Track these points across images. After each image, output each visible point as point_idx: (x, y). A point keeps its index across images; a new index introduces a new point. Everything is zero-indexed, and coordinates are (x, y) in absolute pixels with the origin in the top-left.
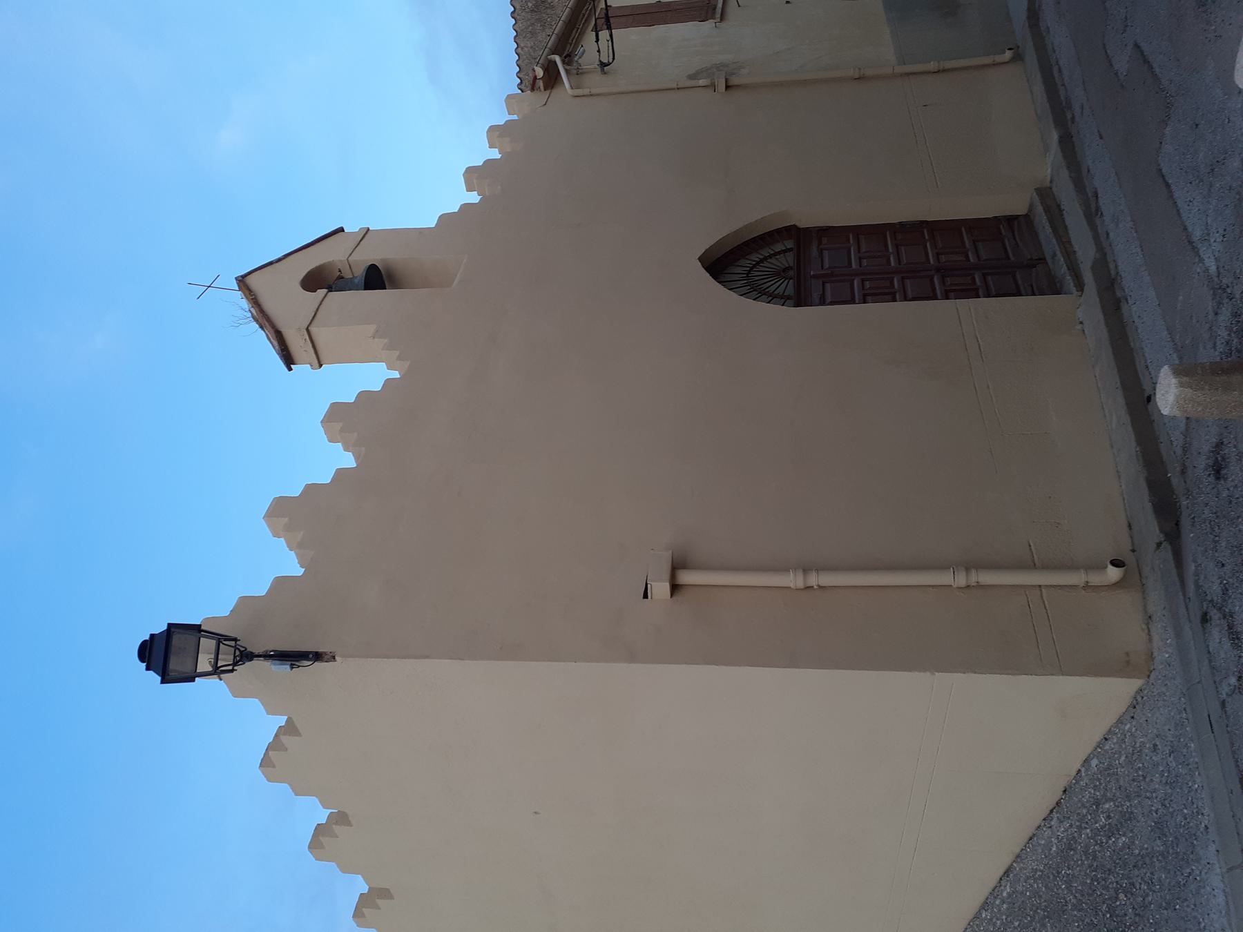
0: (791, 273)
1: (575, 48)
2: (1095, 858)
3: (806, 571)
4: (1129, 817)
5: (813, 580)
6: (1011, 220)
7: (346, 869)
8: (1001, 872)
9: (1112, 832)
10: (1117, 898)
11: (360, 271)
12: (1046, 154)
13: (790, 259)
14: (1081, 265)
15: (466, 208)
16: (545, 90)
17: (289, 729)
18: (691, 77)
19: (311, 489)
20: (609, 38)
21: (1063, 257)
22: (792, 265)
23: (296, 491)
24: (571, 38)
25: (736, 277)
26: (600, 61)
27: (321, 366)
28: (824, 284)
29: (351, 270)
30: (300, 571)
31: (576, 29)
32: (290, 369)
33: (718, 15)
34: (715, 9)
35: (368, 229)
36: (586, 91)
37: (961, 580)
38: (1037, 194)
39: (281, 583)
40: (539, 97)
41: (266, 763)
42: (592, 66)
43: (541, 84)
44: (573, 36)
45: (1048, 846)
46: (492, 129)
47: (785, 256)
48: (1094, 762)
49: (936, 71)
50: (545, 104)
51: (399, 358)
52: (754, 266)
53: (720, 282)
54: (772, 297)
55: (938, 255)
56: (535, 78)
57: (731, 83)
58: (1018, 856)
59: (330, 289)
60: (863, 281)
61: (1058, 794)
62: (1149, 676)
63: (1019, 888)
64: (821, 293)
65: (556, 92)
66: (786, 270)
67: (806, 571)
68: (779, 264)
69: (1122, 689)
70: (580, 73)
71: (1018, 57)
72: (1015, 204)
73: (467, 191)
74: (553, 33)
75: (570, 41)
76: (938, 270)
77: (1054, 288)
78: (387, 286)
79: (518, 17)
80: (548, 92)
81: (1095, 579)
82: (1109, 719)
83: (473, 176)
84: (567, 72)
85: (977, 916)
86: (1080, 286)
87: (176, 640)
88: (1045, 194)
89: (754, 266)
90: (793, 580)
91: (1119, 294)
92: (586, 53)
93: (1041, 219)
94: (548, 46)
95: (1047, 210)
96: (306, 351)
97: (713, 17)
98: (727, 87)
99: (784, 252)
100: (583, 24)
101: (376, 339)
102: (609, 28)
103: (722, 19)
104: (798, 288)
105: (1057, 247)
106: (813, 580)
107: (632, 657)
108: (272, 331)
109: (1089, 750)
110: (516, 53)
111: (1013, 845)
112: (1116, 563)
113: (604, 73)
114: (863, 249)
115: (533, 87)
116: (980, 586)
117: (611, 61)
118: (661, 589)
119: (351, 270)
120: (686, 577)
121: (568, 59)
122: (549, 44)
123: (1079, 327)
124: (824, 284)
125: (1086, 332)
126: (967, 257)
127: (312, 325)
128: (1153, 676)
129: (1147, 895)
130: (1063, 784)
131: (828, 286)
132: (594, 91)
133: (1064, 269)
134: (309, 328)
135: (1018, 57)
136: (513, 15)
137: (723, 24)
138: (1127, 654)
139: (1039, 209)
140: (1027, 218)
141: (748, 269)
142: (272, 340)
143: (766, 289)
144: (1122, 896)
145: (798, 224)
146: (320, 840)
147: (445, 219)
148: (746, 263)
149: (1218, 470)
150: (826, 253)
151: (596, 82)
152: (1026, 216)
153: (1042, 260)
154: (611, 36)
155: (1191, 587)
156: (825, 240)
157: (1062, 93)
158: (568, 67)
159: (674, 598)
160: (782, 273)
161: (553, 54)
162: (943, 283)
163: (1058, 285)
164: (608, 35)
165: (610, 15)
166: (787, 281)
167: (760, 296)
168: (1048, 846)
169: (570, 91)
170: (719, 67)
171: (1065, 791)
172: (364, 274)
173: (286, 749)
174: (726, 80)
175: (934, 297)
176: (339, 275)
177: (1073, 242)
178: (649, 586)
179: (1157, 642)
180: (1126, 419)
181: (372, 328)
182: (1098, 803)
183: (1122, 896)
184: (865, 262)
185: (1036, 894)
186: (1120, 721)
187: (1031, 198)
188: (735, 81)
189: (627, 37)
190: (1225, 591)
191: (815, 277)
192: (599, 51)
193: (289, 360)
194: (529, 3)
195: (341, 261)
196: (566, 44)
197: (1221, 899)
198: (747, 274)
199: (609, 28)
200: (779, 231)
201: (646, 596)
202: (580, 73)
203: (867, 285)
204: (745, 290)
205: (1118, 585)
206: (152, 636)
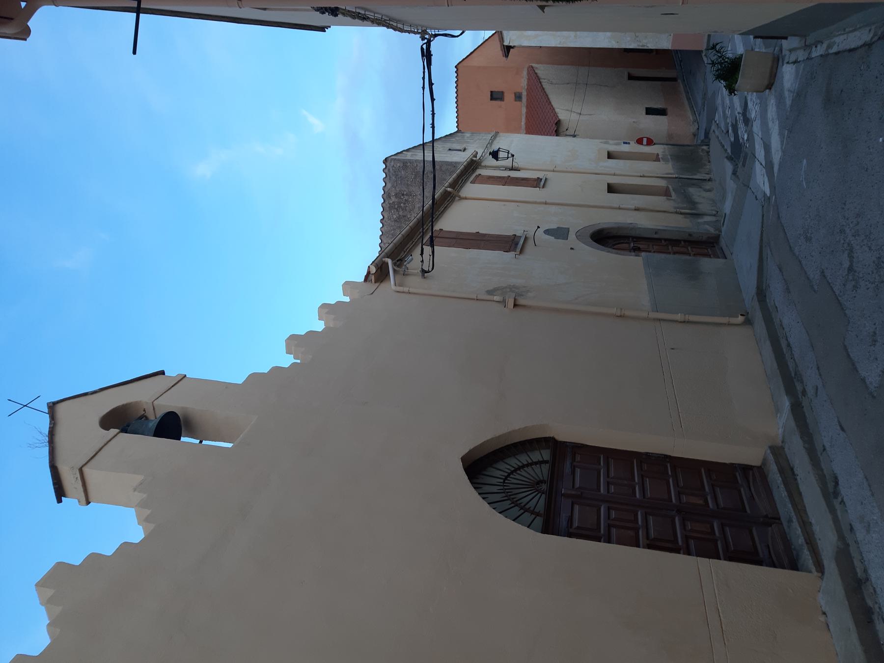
0: (544, 487)
12: (777, 414)
13: (544, 471)
14: (819, 542)
16: (375, 282)
18: (490, 292)
20: (431, 253)
21: (801, 528)
22: (546, 479)
24: (406, 248)
25: (494, 481)
26: (422, 269)
27: (88, 503)
29: (155, 412)
31: (411, 242)
32: (59, 501)
33: (518, 250)
34: (517, 244)
35: (185, 376)
36: (406, 289)
38: (772, 453)
40: (372, 286)
42: (416, 271)
43: (373, 278)
44: (408, 246)
46: (324, 306)
47: (540, 466)
49: (682, 321)
50: (372, 294)
52: (512, 472)
55: (679, 494)
57: (518, 303)
60: (609, 509)
65: (384, 286)
66: (540, 482)
68: (534, 475)
72: (755, 461)
73: (287, 353)
75: (405, 250)
79: (385, 223)
80: (377, 284)
84: (395, 271)
86: (820, 567)
88: (777, 451)
92: (413, 261)
93: (773, 470)
94: (385, 251)
95: (781, 471)
96: (76, 488)
97: (514, 250)
98: (515, 305)
100: (419, 239)
101: (136, 493)
102: (432, 246)
103: (521, 252)
105: (793, 514)
110: (380, 246)
113: (424, 277)
114: (612, 474)
117: (430, 270)
119: (155, 412)
122: (388, 249)
123: (822, 618)
125: (831, 627)
126: (706, 501)
131: (577, 507)
132: (411, 290)
133: (801, 540)
134: (83, 469)
135: (748, 322)
136: (382, 221)
137: (521, 257)
139: (771, 457)
141: (509, 471)
143: (519, 500)
145: (557, 438)
147: (254, 378)
150: (578, 471)
151: (415, 283)
152: (759, 468)
153: (777, 518)
154: (433, 252)
156: (578, 458)
157: (791, 365)
158: (396, 268)
161: (388, 258)
162: (683, 526)
163: (795, 553)
164: (431, 251)
166: (540, 494)
167: (513, 507)
169: (393, 287)
170: (512, 288)
174: (515, 300)
176: (143, 414)
177: (809, 514)
187: (765, 453)
188: (521, 301)
191: (567, 496)
192: (422, 261)
193: (60, 493)
194: (394, 216)
195: (147, 403)
198: (505, 480)
199: (432, 246)
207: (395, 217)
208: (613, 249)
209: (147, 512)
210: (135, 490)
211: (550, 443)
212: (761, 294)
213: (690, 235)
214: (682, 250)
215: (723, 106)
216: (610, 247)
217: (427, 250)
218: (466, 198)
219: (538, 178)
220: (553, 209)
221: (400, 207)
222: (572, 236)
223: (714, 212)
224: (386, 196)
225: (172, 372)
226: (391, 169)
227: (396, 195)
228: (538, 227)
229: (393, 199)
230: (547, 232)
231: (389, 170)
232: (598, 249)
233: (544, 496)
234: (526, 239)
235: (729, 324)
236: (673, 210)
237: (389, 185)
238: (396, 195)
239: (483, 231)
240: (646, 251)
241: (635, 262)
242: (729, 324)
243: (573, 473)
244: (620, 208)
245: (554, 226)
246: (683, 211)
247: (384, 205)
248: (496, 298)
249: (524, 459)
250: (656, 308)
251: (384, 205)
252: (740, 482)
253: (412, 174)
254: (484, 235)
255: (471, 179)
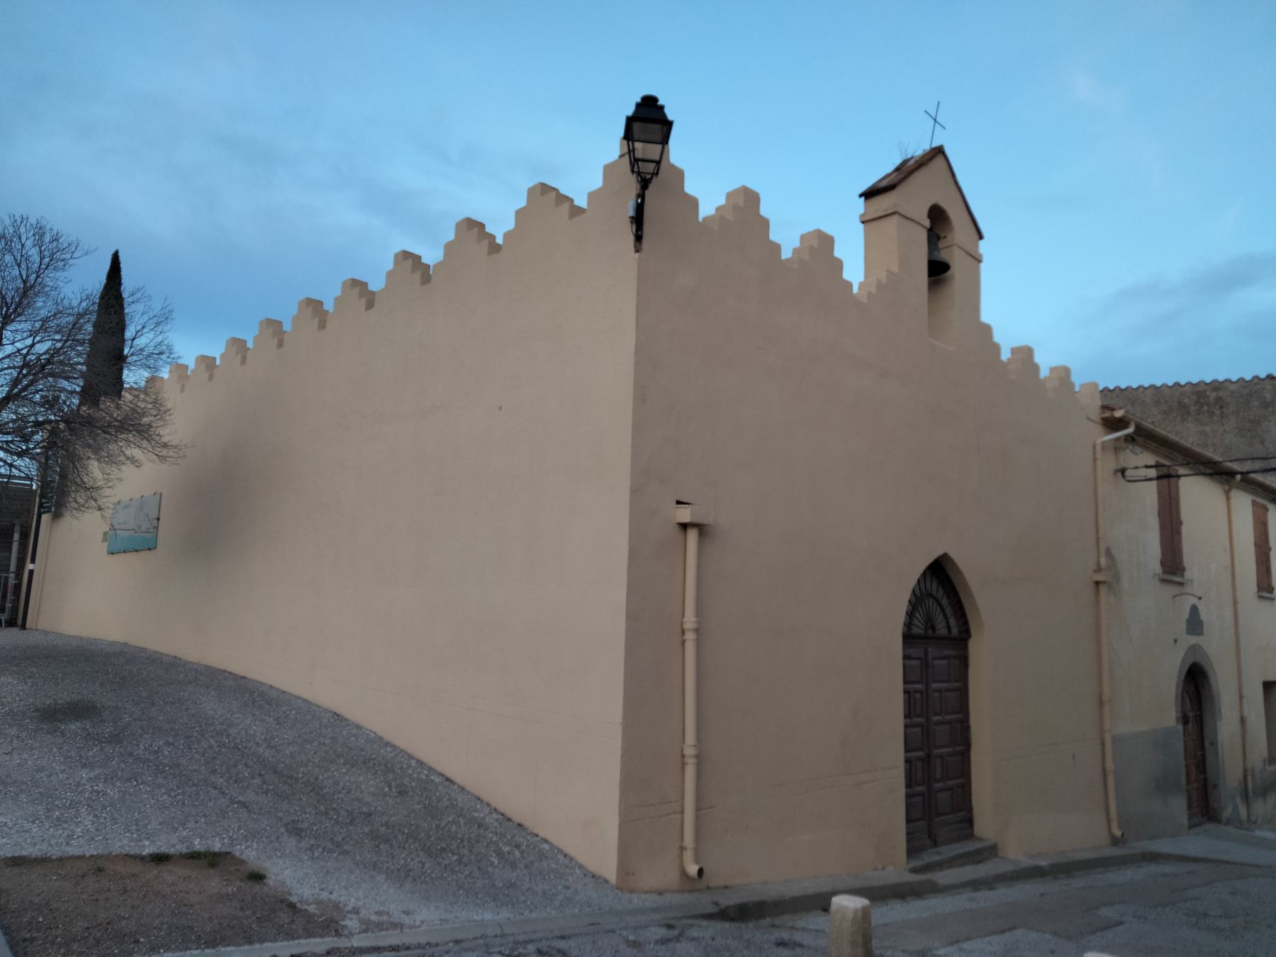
1: (1140, 446)
2: (478, 842)
3: (697, 630)
4: (513, 866)
5: (690, 636)
6: (970, 821)
7: (449, 247)
8: (448, 774)
9: (500, 854)
10: (453, 854)
11: (944, 255)
13: (942, 631)
15: (997, 348)
17: (576, 211)
18: (1108, 552)
19: (765, 223)
22: (938, 632)
23: (764, 211)
25: (928, 585)
27: (863, 222)
28: (920, 659)
30: (700, 219)
32: (861, 196)
33: (1166, 577)
34: (1173, 573)
36: (1099, 456)
37: (690, 751)
39: (693, 203)
40: (1096, 414)
41: (544, 189)
43: (1107, 414)
45: (476, 810)
46: (1066, 371)
48: (546, 847)
51: (870, 294)
52: (937, 601)
53: (925, 572)
54: (910, 615)
55: (941, 756)
56: (1113, 410)
58: (463, 789)
59: (930, 230)
60: (921, 692)
61: (517, 818)
62: (618, 888)
63: (440, 788)
64: (913, 656)
65: (1099, 429)
66: (933, 627)
67: (697, 630)
69: (609, 870)
70: (1117, 450)
71: (1115, 842)
72: (985, 823)
74: (1156, 426)
76: (929, 755)
77: (913, 850)
78: (931, 278)
80: (1100, 421)
81: (688, 856)
82: (582, 859)
83: (1025, 355)
84: (1117, 439)
85: (410, 757)
87: (657, 128)
89: (937, 601)
90: (690, 620)
91: (909, 899)
93: (970, 846)
95: (978, 851)
97: (1165, 572)
98: (1097, 583)
99: (949, 627)
102: (1159, 478)
103: (1163, 581)
104: (918, 637)
106: (690, 636)
107: (635, 491)
108: (895, 181)
109: (556, 843)
111: (472, 786)
112: (701, 872)
113: (1116, 471)
114: (948, 694)
115: (1105, 408)
116: (684, 765)
117: (1128, 478)
118: (685, 515)
120: (692, 535)
121: (1130, 439)
124: (920, 659)
127: (902, 220)
128: (618, 892)
129: (462, 874)
130: (528, 824)
132: (1099, 463)
135: (1115, 842)
138: (633, 874)
139: (979, 845)
140: (970, 836)
142: (888, 180)
144: (456, 857)
146: (473, 228)
147: (987, 330)
148: (940, 594)
149: (781, 944)
150: (945, 662)
151: (1108, 463)
153: (935, 844)
155: (690, 922)
156: (957, 662)
158: (1123, 439)
159: (677, 526)
160: (931, 626)
162: (918, 759)
165: (1172, 479)
168: (476, 810)
170: (1117, 576)
171: (520, 825)
172: (942, 260)
173: (557, 206)
174: (1104, 582)
175: (907, 750)
178: (687, 506)
179: (643, 896)
180: (810, 891)
181: (895, 269)
182: (518, 846)
183: (456, 857)
184: (937, 695)
185: (439, 799)
186: (581, 867)
188: (1103, 589)
189: (1149, 494)
190: (693, 939)
191: (926, 652)
192: (1136, 468)
193: (869, 195)
196: (1145, 438)
197: (479, 918)
199: (1159, 478)
200: (966, 623)
201: (679, 502)
202: (1117, 450)
203: (918, 696)
204: (918, 592)
205: (684, 873)
206: (662, 108)
207: (1186, 400)
208: (1182, 692)
209: (874, 291)
210: (888, 271)
211: (965, 634)
212: (1154, 858)
213: (1215, 786)
214: (1193, 777)
215: (1247, 796)
216: (1183, 688)
217: (1152, 473)
218: (1228, 499)
219: (1273, 589)
220: (1228, 613)
221: (1202, 405)
222: (1193, 640)
223: (1253, 819)
224: (1216, 386)
225: (983, 246)
226: (1258, 387)
227: (1219, 399)
228: (1200, 598)
229: (1213, 395)
230: (1194, 609)
231: (1256, 384)
232: (1179, 676)
233: (922, 632)
234: (1181, 584)
235: (1109, 821)
236: (1249, 765)
237: (1234, 387)
238: (1219, 399)
239: (1184, 529)
240: (1184, 732)
241: (1168, 717)
242: (1109, 821)
243: (944, 658)
244: (1241, 697)
245: (1203, 615)
246: (1249, 778)
247: (1202, 384)
248: (1103, 561)
249: (949, 611)
250: (1117, 740)
251: (1202, 384)
252: (959, 814)
253: (1255, 416)
254: (1179, 533)
255: (1260, 501)
